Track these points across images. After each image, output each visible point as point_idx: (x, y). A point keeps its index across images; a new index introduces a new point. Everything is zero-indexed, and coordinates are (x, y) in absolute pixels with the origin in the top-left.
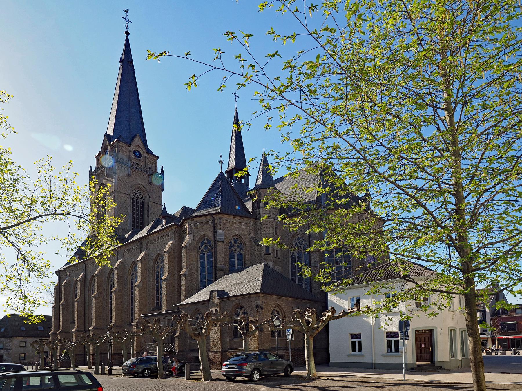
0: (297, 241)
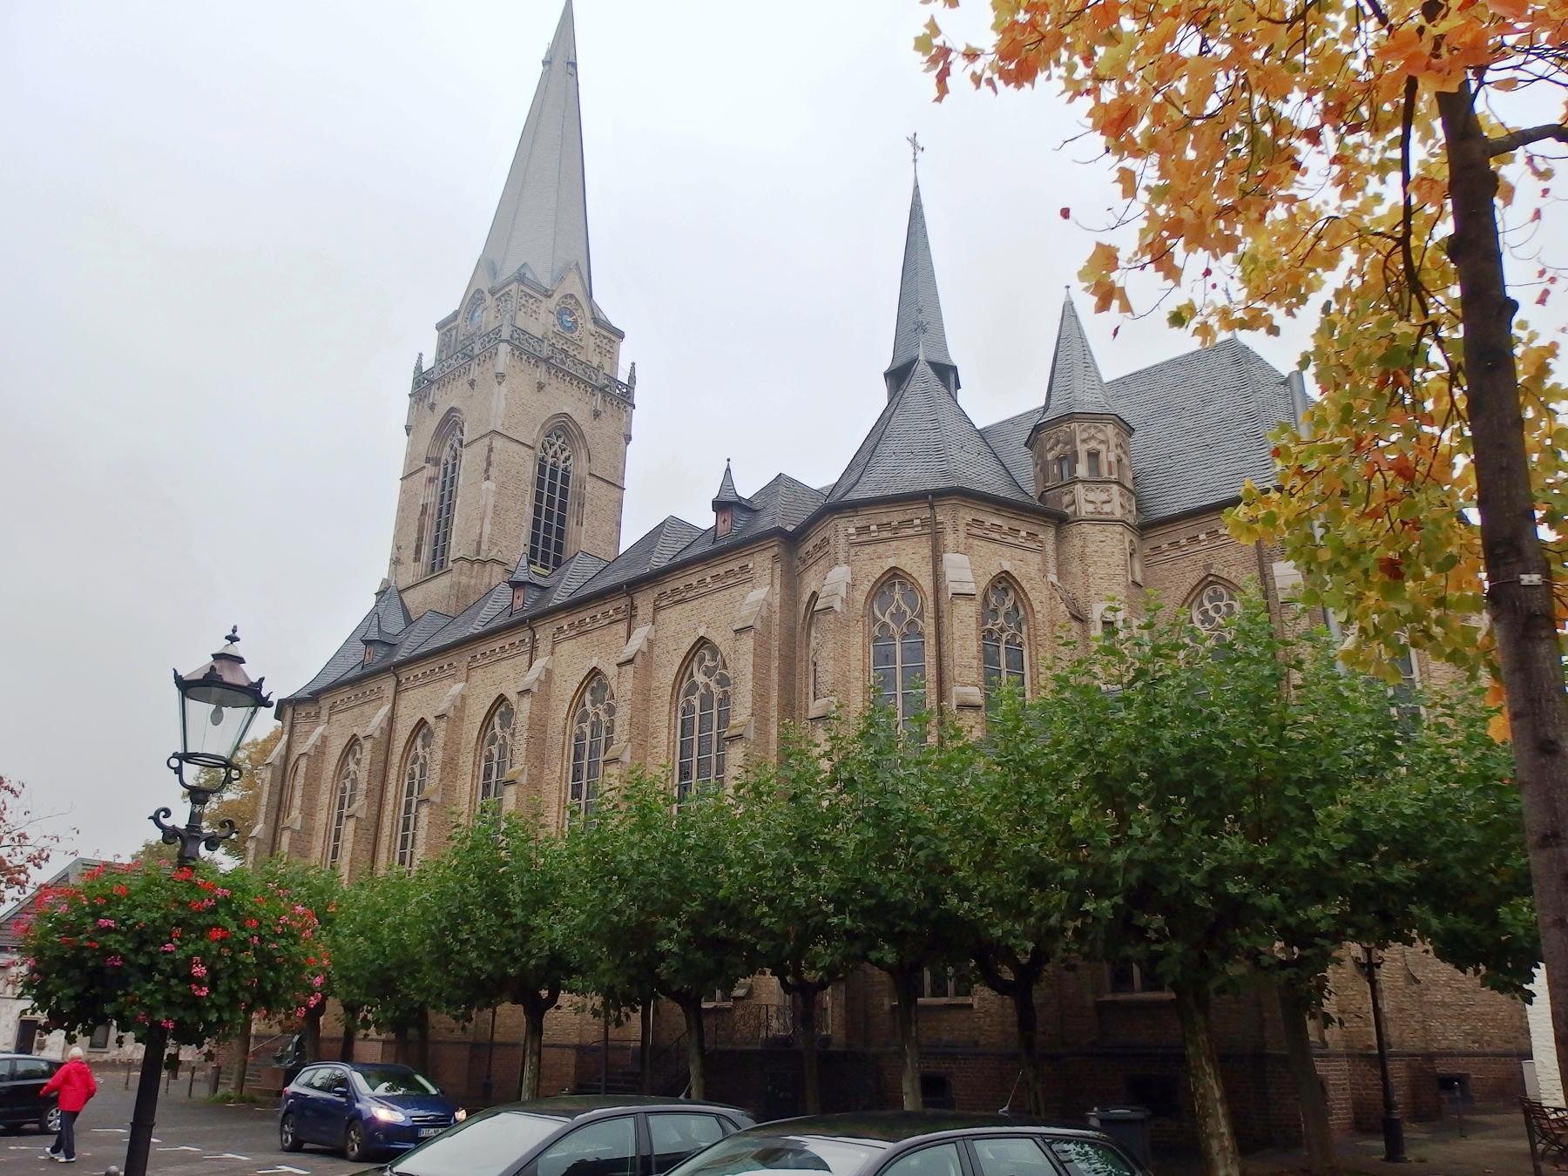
0: (1208, 605)
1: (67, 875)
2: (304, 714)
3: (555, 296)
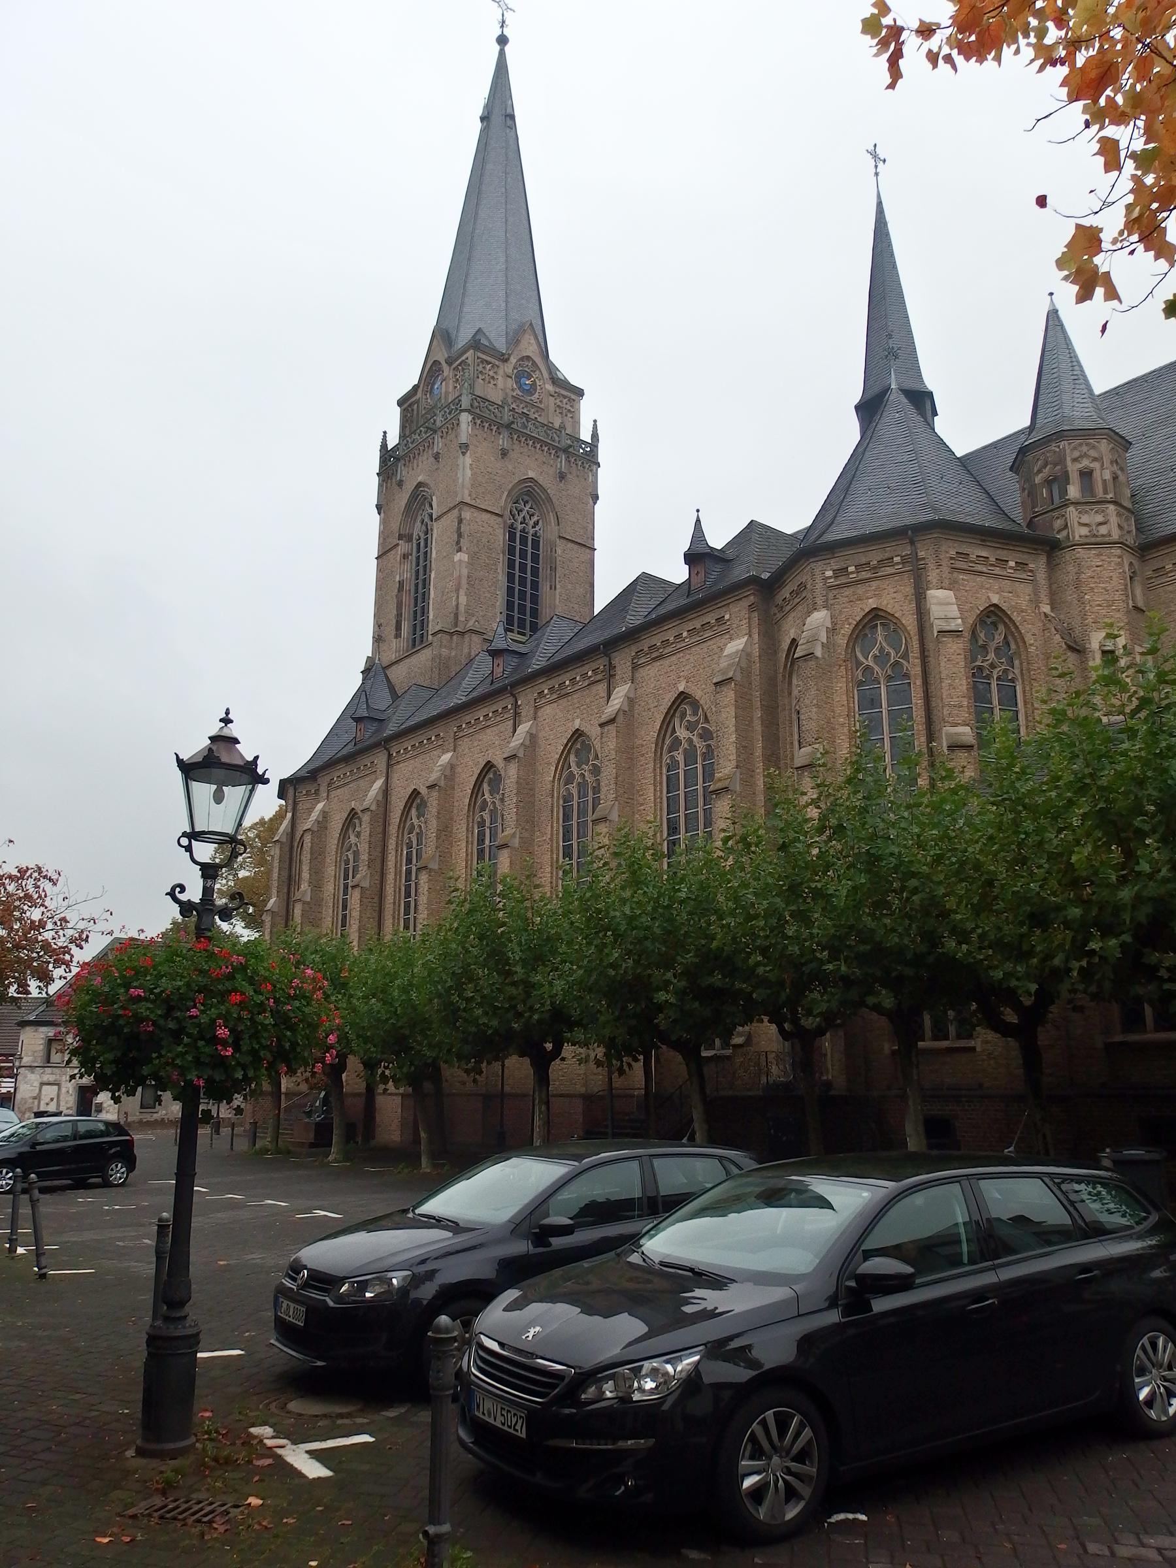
2: (304, 792)
3: (512, 358)
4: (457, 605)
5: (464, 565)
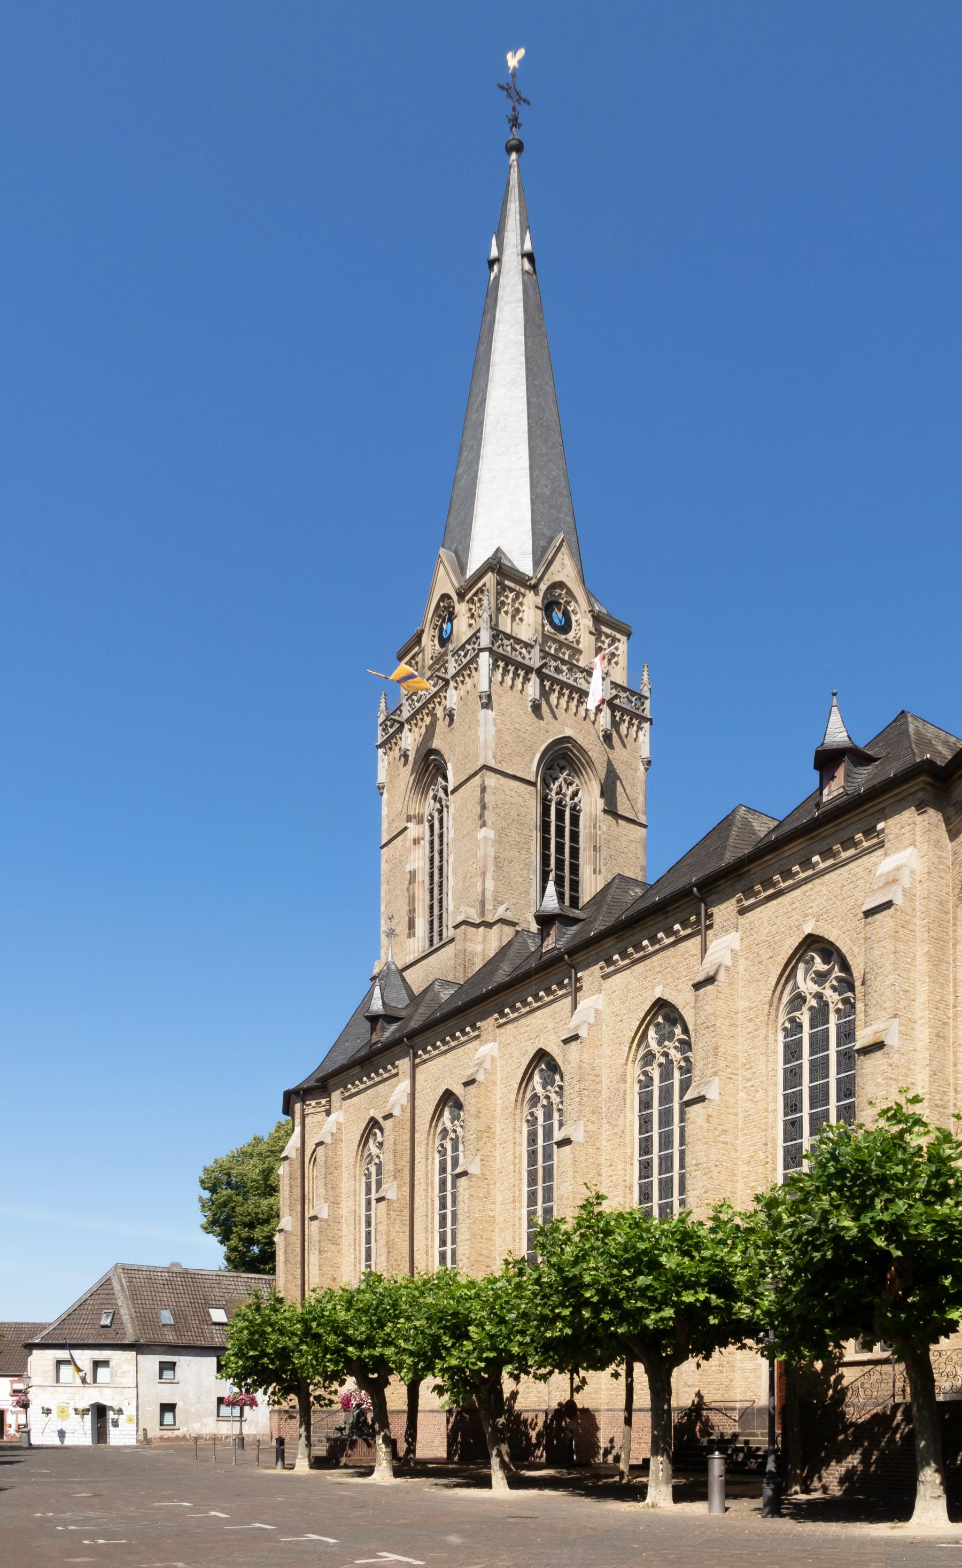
1: (109, 1279)
4: (484, 890)
5: (490, 843)
